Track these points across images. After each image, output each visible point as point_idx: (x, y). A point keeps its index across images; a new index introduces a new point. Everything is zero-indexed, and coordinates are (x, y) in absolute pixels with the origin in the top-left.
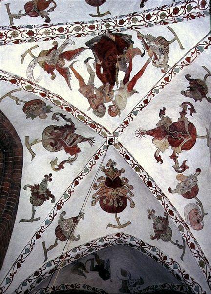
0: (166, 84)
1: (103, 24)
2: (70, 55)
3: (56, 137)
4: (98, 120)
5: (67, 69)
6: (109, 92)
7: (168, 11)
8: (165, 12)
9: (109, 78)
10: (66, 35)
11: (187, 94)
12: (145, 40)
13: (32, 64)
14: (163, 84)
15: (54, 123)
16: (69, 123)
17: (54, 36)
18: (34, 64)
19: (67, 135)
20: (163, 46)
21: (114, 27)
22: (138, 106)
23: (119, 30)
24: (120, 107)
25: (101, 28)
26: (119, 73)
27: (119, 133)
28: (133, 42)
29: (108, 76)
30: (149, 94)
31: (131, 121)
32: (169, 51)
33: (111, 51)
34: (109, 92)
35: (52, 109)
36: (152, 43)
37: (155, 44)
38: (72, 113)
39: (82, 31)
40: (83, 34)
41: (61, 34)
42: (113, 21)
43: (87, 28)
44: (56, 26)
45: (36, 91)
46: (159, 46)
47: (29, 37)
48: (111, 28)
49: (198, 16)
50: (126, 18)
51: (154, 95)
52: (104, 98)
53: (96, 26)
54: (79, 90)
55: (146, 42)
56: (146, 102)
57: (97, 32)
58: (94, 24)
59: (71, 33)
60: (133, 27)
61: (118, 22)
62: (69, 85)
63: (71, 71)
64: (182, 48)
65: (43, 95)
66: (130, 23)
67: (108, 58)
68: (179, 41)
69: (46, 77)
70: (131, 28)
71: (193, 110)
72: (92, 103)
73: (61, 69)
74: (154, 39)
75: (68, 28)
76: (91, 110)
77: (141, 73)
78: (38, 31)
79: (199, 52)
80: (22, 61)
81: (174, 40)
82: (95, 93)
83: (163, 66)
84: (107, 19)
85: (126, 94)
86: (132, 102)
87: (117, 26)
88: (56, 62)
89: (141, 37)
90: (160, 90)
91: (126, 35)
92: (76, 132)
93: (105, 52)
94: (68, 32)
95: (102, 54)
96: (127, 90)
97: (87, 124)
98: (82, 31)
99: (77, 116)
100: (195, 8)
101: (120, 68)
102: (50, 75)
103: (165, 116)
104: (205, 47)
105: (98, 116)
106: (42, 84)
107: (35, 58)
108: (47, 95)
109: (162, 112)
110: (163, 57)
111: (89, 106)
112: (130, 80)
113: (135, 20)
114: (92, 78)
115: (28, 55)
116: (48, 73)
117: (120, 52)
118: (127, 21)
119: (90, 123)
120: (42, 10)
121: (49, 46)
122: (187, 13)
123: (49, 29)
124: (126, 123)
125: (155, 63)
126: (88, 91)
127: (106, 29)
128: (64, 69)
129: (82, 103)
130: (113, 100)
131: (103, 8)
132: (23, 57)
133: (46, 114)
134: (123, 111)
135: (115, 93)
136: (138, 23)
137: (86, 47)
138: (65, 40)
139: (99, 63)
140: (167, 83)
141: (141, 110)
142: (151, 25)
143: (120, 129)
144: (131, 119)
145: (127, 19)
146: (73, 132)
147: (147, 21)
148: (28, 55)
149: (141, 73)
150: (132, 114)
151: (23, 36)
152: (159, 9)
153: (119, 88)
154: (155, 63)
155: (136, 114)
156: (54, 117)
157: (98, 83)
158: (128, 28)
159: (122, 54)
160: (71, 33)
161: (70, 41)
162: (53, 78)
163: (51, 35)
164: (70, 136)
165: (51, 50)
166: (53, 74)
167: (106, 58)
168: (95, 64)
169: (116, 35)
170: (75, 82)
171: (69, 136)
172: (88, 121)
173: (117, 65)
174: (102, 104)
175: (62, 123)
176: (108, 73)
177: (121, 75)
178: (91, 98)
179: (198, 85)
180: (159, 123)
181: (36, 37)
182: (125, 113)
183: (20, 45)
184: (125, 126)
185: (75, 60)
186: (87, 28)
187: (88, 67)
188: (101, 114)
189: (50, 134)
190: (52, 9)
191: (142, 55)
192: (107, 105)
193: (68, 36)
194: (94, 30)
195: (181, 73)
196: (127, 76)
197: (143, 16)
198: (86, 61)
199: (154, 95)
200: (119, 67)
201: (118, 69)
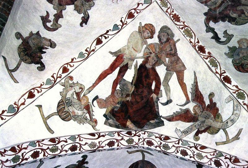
0: (67, 64)
1: (137, 144)
2: (184, 116)
3: (238, 6)
4: (169, 23)
5: (193, 100)
6: (149, 57)
7: (46, 154)
8: (51, 153)
9: (145, 75)
10: (180, 145)
11: (48, 43)
12: (88, 118)
13: (230, 123)
14: (72, 64)
15: (232, 28)
16: (212, 24)
17: (193, 149)
18: (227, 122)
19: (220, 6)
20: (66, 109)
21: (122, 139)
22: (110, 37)
23: (116, 134)
24: (138, 36)
25: (139, 140)
26: (132, 78)
27: (143, 3)
28: (105, 116)
29: (147, 76)
30: (92, 52)
31: (124, 16)
32: (59, 103)
33: (135, 107)
34: (149, 57)
35: (227, 51)
36: (80, 113)
37: (76, 111)
38: (198, 42)
39: (161, 143)
40: (161, 140)
41: (185, 149)
42: (122, 146)
43: (156, 144)
44: (189, 160)
45: (235, 88)
46: (71, 109)
47: (220, 161)
48: (126, 138)
49: (5, 151)
50: (104, 148)
51: (86, 50)
52: (158, 50)
53: (145, 143)
54: (185, 68)
55: (88, 115)
56: (99, 42)
57: (146, 136)
58: (147, 146)
59: (173, 146)
60: (97, 136)
61: (116, 144)
62: (196, 78)
63: (190, 96)
64: (40, 107)
65: (227, 80)
66: (99, 142)
67: (142, 99)
68: (42, 115)
69: (220, 100)
70: (99, 137)
71: (45, 19)
72: (173, 48)
73: (200, 103)
74: (76, 118)
75: (176, 151)
76: (175, 39)
77: (102, 76)
78: (209, 163)
79: (15, 106)
80: (240, 132)
81: (49, 117)
82: (167, 59)
83: (69, 83)
84: (130, 148)
85: (127, 52)
86: (118, 42)
87: (117, 140)
88: (203, 114)
89: (93, 122)
90: (76, 56)
92: (206, 9)
93: (144, 107)
94: (177, 147)
95: (148, 106)
96: (125, 57)
97: (184, 23)
98: (161, 143)
99: (194, 37)
100: (7, 161)
101: (130, 86)
102: (215, 100)
103: (82, 15)
104: (6, 112)
105: (169, 29)
106: (226, 94)
107: (224, 130)
108: (222, 77)
109: (85, 20)
110: (69, 96)
111: (178, 45)
112: (118, 68)
113: (93, 145)
114: (167, 79)
115: (231, 137)
116: (215, 104)
117: (124, 105)
118: (103, 145)
119: (178, 23)
121: (205, 139)
122: (20, 154)
123: (197, 159)
124: (131, 16)
125: (81, 88)
126: (175, 64)
127: (133, 138)
128: (197, 101)
129: (185, 51)
130: (145, 46)
131: (137, 157)
132: (237, 138)
133: (237, 46)
134: (135, 30)
135: (141, 54)
137: (165, 121)
138: (185, 139)
139: (154, 96)
140: (66, 66)
141: (108, 31)
142: (73, 138)
143: (141, 7)
144: (123, 20)
145: (103, 147)
146: (210, 10)
147: (76, 144)
148: (231, 137)
149: (102, 76)
150: (120, 27)
152: (59, 156)
153: (135, 60)
154: (81, 88)
155: (116, 27)
156: (229, 37)
157: (161, 70)
158: (103, 136)
159: (123, 102)
160: (173, 146)
161: (180, 134)
162: (211, 95)
163: (196, 152)
164: (216, 4)
165: (204, 131)
166: (211, 101)
167: (145, 100)
168: (159, 96)
169: (124, 126)
170: (189, 81)
171: (218, 4)
172: (181, 27)
173: (132, 89)
174: (162, 43)
175: (220, 27)
176: (145, 81)
177: (130, 76)
178: (173, 54)
179: (30, 56)
180: (91, 7)
181: (213, 156)
182: (132, 26)
183: (233, 153)
184: (133, 11)
185: (181, 107)
186: (156, 144)
187: (169, 93)
188: (165, 30)
189: (244, 13)
191: (96, 98)
192: (155, 40)
193: (178, 143)
194: (148, 139)
195: (47, 75)
196: (122, 74)
197: (82, 149)
198: (169, 102)
199: (86, 50)
200: (130, 86)
201: (132, 83)
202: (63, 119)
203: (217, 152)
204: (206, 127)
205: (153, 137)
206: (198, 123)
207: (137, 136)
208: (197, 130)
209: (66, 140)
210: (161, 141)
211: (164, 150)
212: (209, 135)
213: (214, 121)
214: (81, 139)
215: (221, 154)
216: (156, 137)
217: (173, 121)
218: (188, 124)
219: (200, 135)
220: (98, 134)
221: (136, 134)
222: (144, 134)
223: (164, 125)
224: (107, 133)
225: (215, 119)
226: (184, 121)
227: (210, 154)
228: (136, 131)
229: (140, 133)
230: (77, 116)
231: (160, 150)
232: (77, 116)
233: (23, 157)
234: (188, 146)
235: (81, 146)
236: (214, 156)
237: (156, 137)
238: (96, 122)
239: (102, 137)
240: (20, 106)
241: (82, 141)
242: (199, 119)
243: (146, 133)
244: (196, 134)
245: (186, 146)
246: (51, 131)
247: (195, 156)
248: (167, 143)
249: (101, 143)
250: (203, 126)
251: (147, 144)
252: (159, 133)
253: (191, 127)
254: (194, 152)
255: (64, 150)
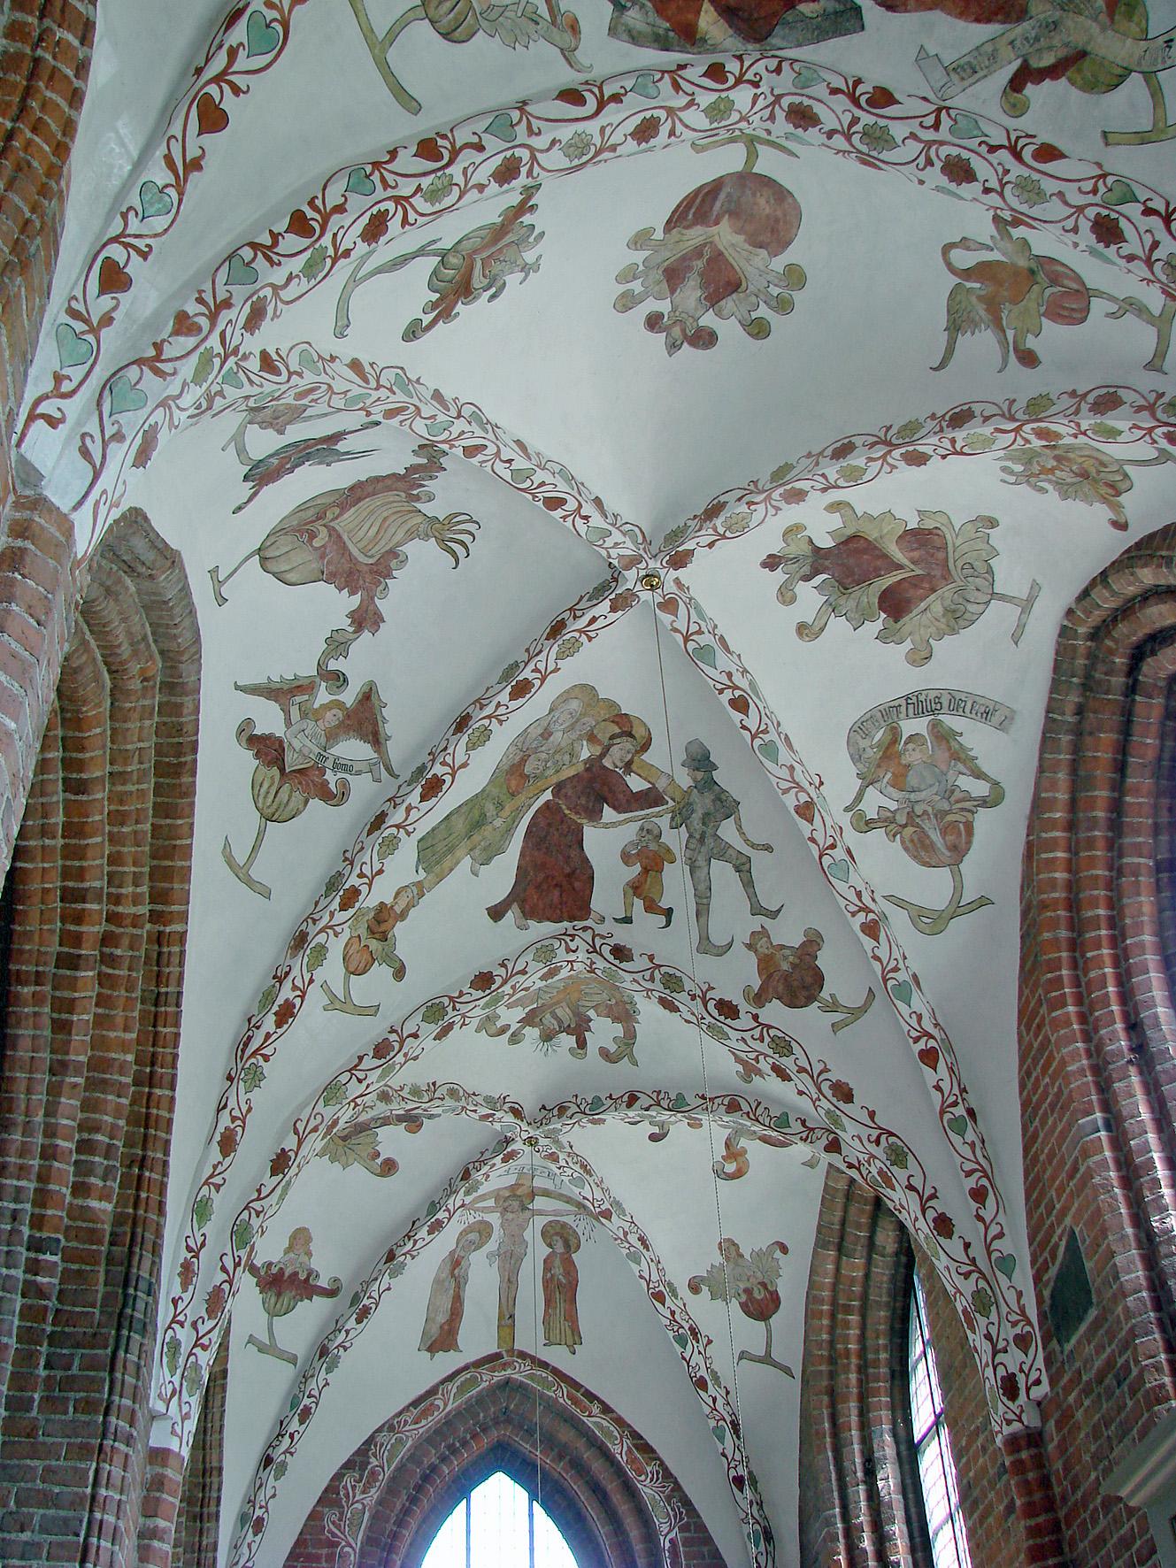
1: (742, 119)
10: (944, 133)
17: (1004, 155)
21: (691, 103)
39: (855, 121)
40: (859, 106)
41: (965, 155)
43: (829, 121)
48: (705, 99)
53: (780, 115)
59: (913, 136)
66: (603, 130)
75: (922, 160)
78: (1070, 224)
87: (671, 111)
91: (635, 38)
94: (929, 144)
98: (855, 121)
104: (242, 54)
120: (1014, 265)
123: (1014, 202)
136: (565, 133)
147: (518, 152)
151: (1148, 240)
158: (616, 98)
160: (913, 136)
161: (939, 76)
163: (1017, 170)
165: (1053, 72)
169: (688, 36)
181: (1091, 199)
186: (829, 121)
190: (965, 243)
193: (936, 126)
194: (797, 100)
202: (446, 36)
203: (1110, 180)
204: (1062, 53)
205: (820, 90)
206: (1025, 27)
207: (749, 82)
208: (1019, 62)
209: (475, 139)
210: (858, 113)
211: (864, 149)
212: (1075, 93)
213: (1103, 29)
214: (535, 124)
215: (1125, 189)
216: (835, 91)
217: (906, 11)
218: (982, 32)
219: (1030, 89)
220: (596, 90)
221: (742, 74)
222: (778, 70)
223: (863, 28)
224: (629, 84)
225: (1112, 20)
226: (962, 15)
227: (1076, 185)
228: (740, 58)
229: (760, 67)
230: (497, 11)
231: (849, 148)
232: (497, 11)
233: (336, 249)
234: (979, 140)
235: (533, 158)
236: (1097, 199)
237: (835, 91)
238: (574, 28)
239: (612, 106)
240: (290, 12)
241: (539, 133)
242: (1033, 10)
243: (785, 65)
244: (1012, 81)
245: (973, 143)
246: (410, 103)
247: (1009, 187)
248: (882, 122)
249: (608, 131)
250: (1050, 48)
251: (788, 118)
252: (844, 69)
253: (989, 48)
254: (1007, 172)
255: (474, 186)
